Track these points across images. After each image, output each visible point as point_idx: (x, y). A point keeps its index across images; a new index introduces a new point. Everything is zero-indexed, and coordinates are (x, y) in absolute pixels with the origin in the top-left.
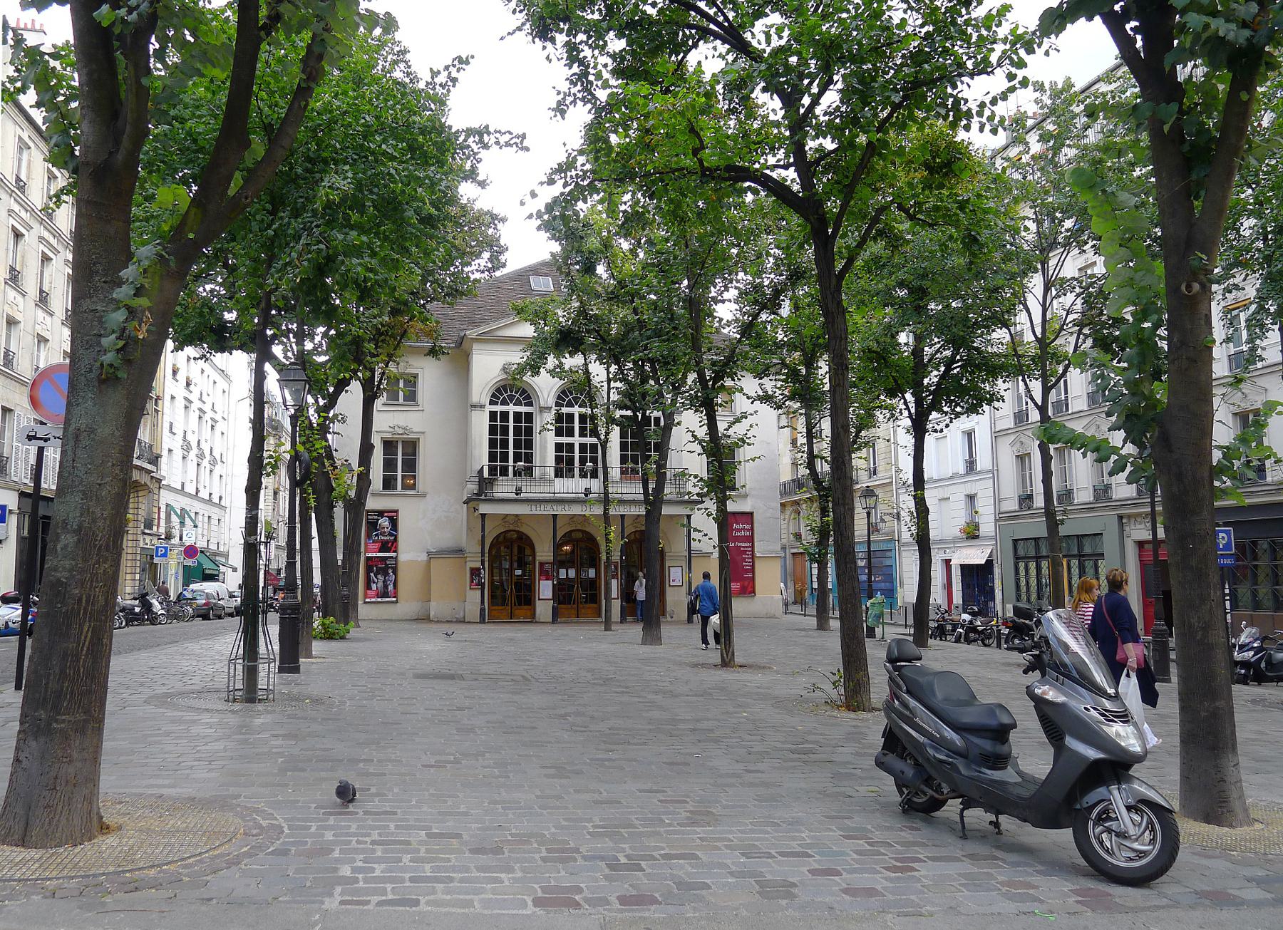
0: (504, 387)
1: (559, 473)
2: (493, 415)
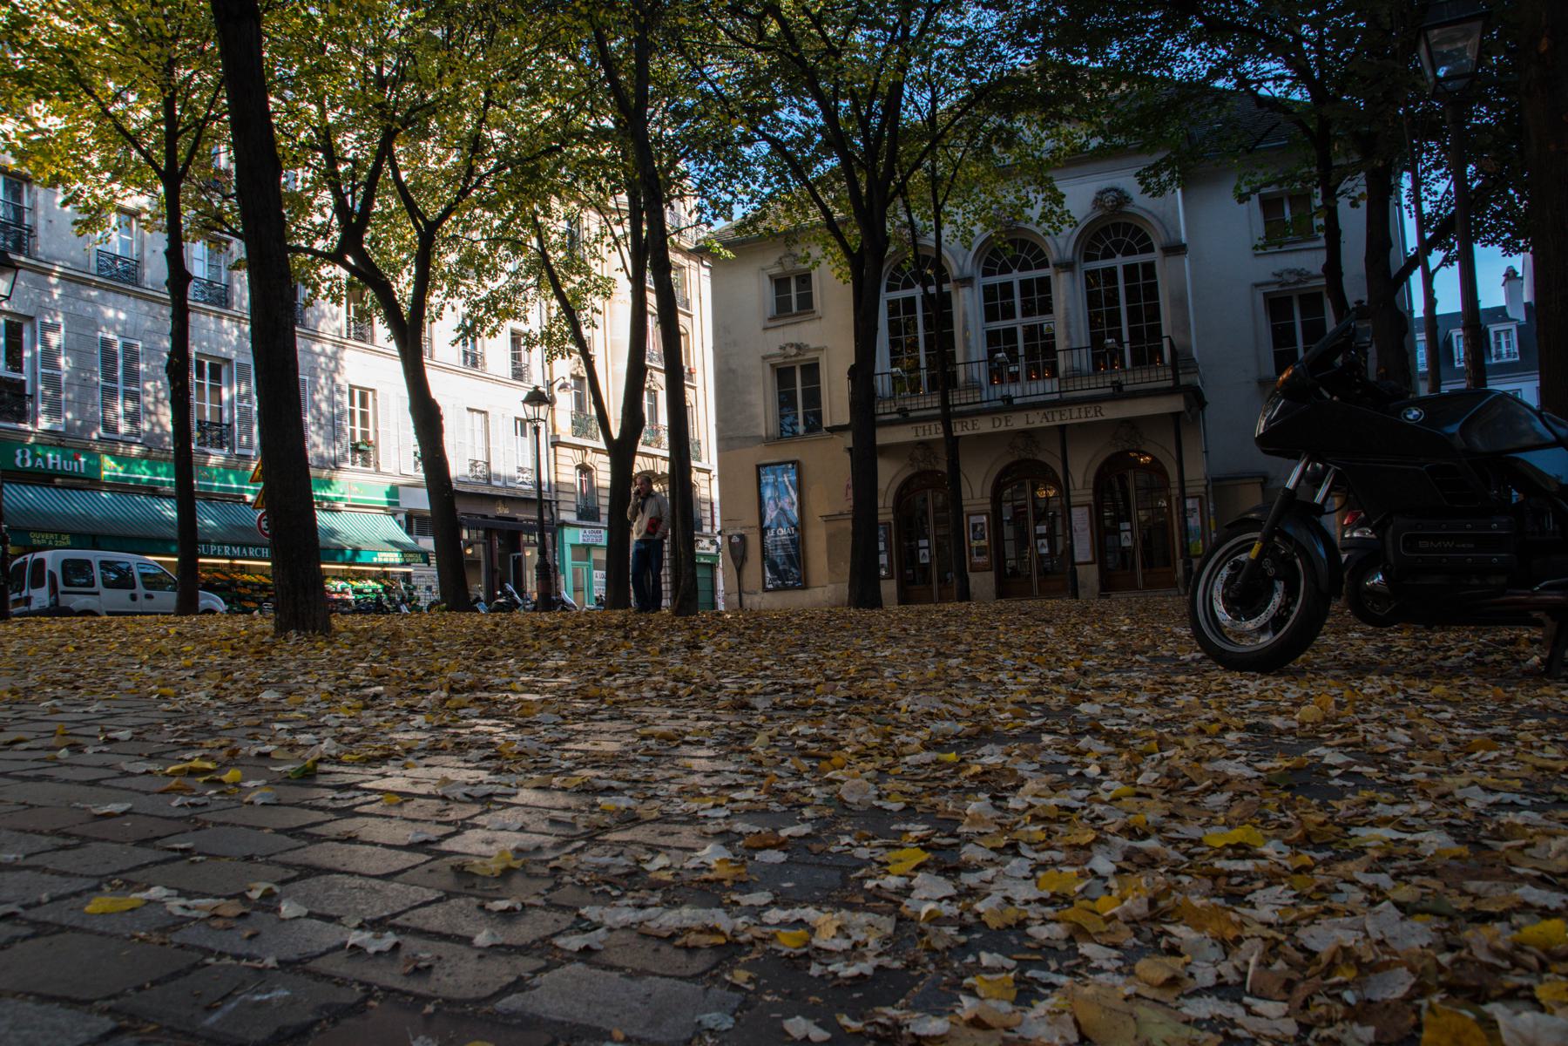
0: (1105, 230)
2: (989, 292)
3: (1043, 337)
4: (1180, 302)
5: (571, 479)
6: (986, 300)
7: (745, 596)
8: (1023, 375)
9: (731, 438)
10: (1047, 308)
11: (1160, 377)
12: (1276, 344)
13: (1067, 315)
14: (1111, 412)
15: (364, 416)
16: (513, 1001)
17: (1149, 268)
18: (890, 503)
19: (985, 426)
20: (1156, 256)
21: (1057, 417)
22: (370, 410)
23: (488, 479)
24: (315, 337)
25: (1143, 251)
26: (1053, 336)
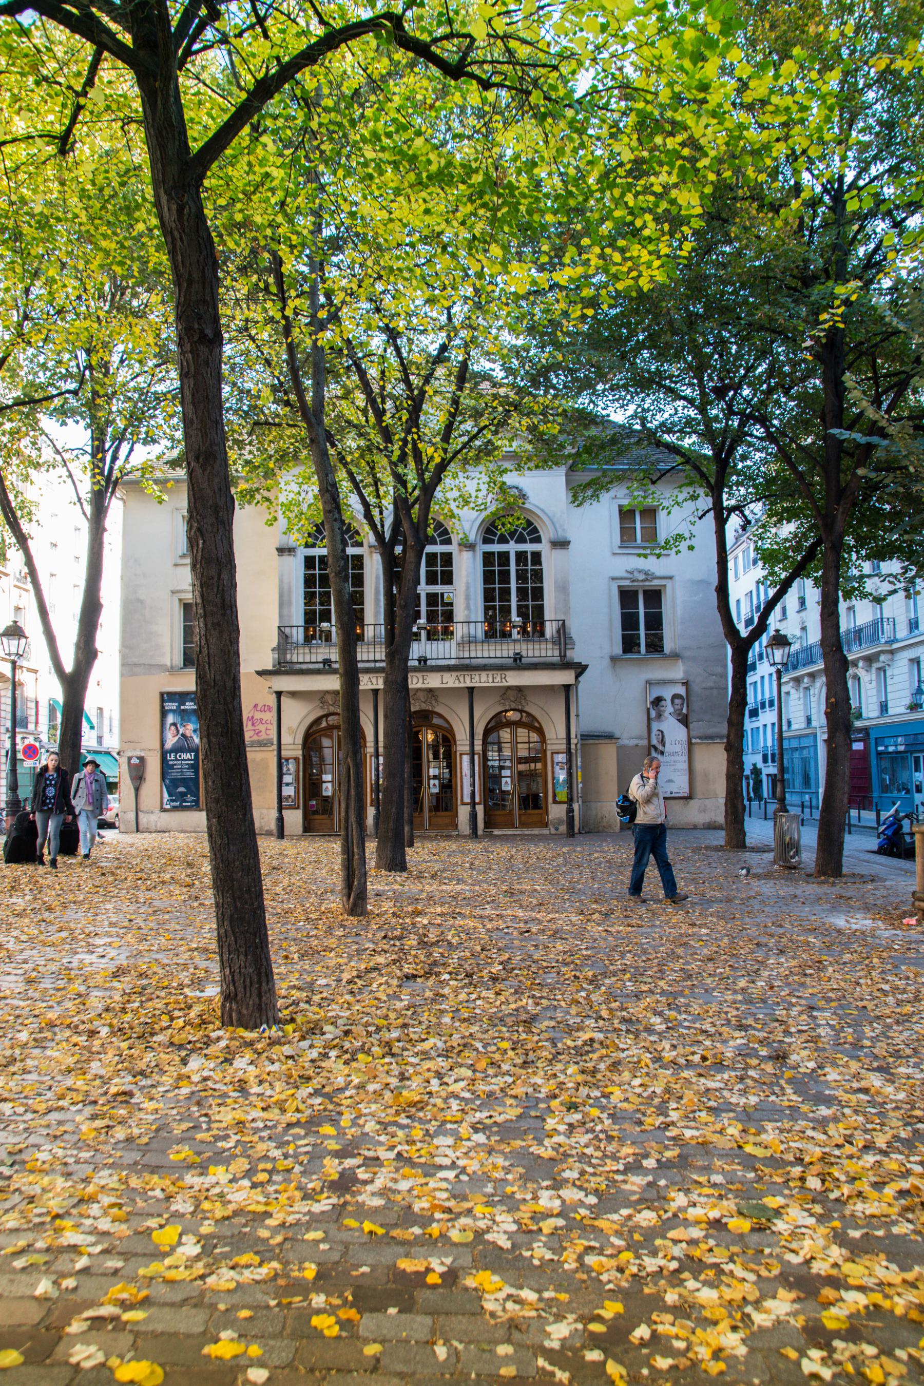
1: (490, 635)
2: (488, 558)
3: (444, 604)
4: (563, 589)
6: (451, 572)
7: (141, 815)
9: (135, 665)
10: (448, 579)
11: (546, 651)
13: (468, 588)
14: (515, 679)
17: (537, 557)
20: (543, 546)
21: (468, 679)
25: (533, 541)
26: (451, 604)
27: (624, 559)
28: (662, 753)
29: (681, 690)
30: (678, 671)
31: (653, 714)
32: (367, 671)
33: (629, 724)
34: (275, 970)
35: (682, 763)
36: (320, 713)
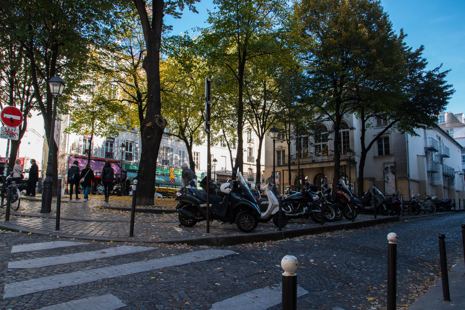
5: (247, 172)
8: (322, 155)
12: (379, 149)
15: (197, 158)
16: (74, 234)
18: (294, 181)
19: (308, 166)
22: (199, 157)
23: (226, 171)
24: (160, 154)
27: (377, 130)
28: (388, 183)
29: (393, 165)
30: (392, 160)
31: (385, 172)
32: (62, 219)
33: (379, 176)
34: (385, 265)
35: (393, 185)
36: (317, 173)
